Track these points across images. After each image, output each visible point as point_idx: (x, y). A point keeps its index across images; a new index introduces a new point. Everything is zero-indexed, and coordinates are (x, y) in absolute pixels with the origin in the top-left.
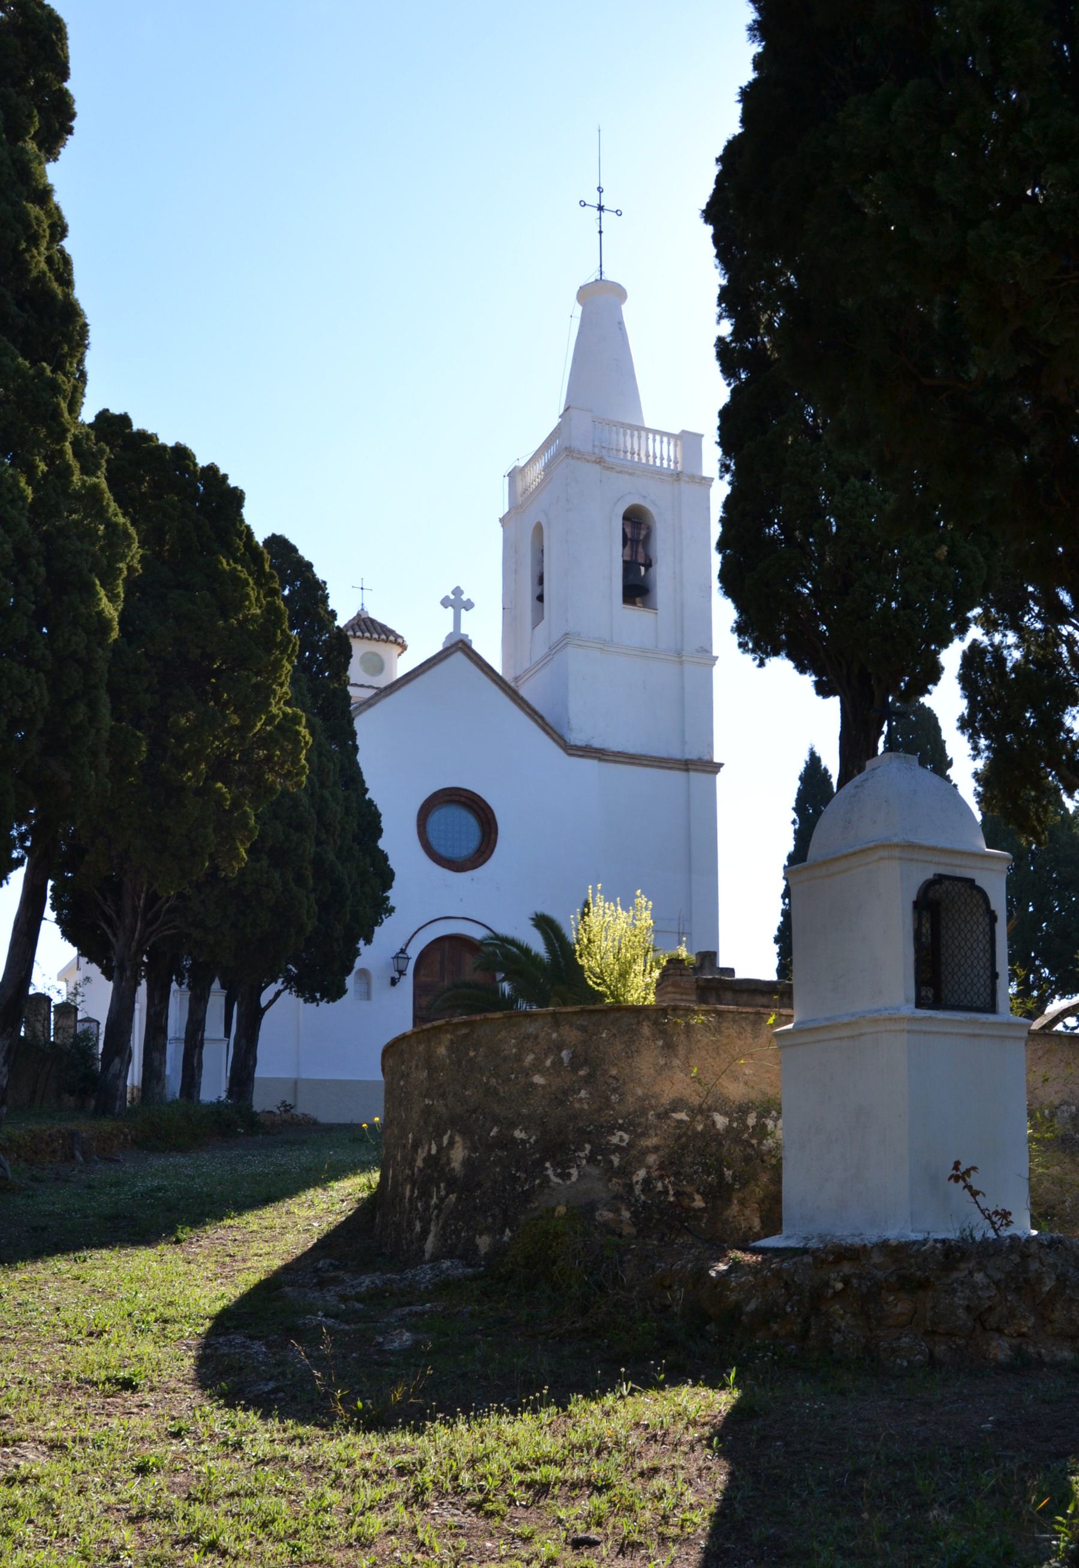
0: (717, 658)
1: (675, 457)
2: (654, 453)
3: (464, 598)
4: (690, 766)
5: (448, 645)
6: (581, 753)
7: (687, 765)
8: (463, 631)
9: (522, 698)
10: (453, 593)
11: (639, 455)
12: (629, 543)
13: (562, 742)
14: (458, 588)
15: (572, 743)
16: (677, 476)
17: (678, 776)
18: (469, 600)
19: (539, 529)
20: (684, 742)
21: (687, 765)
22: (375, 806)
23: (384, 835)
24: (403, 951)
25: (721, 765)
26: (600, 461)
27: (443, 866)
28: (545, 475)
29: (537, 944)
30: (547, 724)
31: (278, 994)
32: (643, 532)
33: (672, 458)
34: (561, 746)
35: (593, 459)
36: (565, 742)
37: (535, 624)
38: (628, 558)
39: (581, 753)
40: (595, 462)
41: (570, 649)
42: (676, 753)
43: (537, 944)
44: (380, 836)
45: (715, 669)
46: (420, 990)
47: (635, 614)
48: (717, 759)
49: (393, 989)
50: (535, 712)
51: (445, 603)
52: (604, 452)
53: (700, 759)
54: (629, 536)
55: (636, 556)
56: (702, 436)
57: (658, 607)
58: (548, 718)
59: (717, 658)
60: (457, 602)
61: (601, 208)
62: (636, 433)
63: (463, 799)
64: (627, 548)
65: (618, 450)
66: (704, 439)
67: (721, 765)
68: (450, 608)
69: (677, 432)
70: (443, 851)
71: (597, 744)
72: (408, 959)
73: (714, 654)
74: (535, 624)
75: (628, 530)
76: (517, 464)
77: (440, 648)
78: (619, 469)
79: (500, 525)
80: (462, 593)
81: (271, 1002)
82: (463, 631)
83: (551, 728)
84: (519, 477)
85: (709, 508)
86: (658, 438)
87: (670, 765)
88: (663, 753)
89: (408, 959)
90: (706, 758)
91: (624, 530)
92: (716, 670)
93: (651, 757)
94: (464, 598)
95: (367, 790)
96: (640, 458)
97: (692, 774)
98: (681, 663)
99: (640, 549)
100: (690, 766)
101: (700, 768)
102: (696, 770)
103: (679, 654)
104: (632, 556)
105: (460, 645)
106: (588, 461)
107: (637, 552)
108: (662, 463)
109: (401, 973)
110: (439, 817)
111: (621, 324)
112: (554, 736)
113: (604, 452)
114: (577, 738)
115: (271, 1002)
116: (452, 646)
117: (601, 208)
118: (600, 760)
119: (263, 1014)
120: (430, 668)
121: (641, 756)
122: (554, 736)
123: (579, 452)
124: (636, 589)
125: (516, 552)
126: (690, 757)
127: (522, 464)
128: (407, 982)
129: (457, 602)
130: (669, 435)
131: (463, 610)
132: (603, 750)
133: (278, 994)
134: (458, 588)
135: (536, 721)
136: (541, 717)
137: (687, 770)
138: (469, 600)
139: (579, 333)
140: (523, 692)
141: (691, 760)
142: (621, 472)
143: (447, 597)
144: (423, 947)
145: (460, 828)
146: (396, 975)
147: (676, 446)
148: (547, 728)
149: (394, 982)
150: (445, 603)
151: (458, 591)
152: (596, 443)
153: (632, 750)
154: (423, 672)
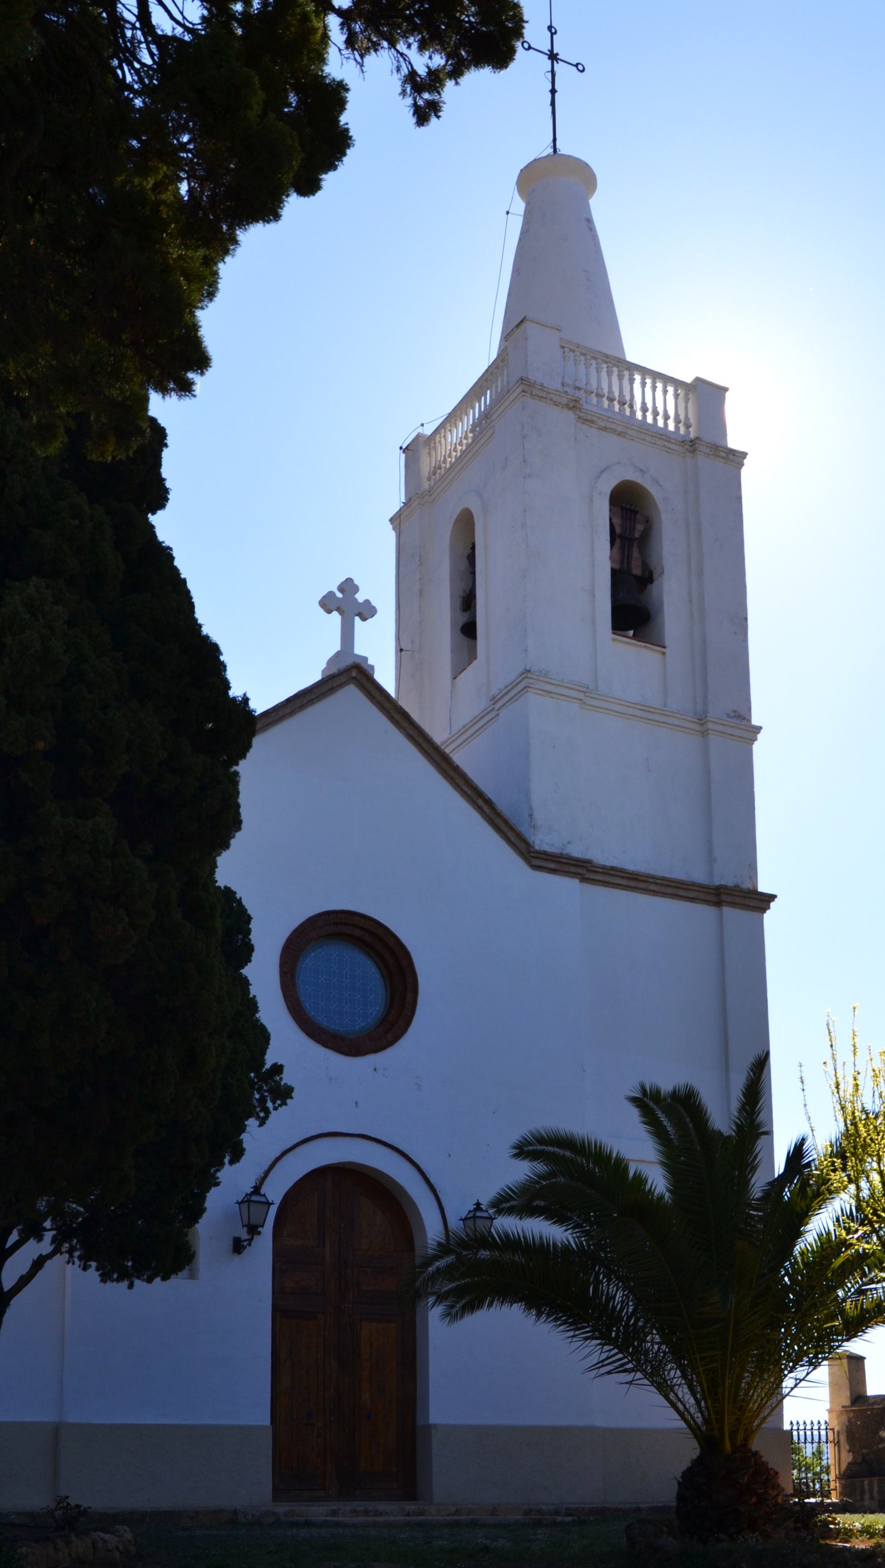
0: (759, 729)
1: (686, 417)
2: (644, 403)
3: (360, 597)
4: (724, 898)
5: (334, 670)
6: (553, 866)
7: (718, 895)
8: (359, 650)
9: (456, 769)
10: (341, 588)
11: (631, 406)
12: (618, 541)
13: (521, 845)
14: (349, 581)
15: (537, 848)
16: (692, 445)
17: (704, 913)
18: (367, 602)
19: (466, 523)
20: (711, 859)
21: (718, 895)
22: (239, 902)
23: (255, 956)
24: (257, 1190)
25: (773, 897)
26: (574, 406)
27: (326, 1045)
28: (474, 439)
29: (643, 1156)
30: (499, 815)
31: (38, 1264)
32: (640, 527)
33: (682, 417)
34: (520, 853)
35: (565, 401)
36: (527, 844)
37: (458, 670)
38: (617, 567)
39: (553, 866)
40: (567, 406)
41: (531, 697)
42: (698, 875)
43: (643, 1156)
44: (248, 960)
45: (757, 747)
46: (283, 1261)
47: (627, 653)
48: (763, 887)
49: (236, 1258)
50: (479, 794)
51: (328, 604)
52: (581, 395)
53: (737, 886)
54: (618, 530)
55: (629, 563)
56: (726, 390)
57: (667, 643)
58: (502, 804)
59: (759, 729)
60: (345, 603)
61: (553, 57)
62: (626, 373)
63: (358, 932)
64: (616, 549)
65: (600, 396)
66: (727, 394)
67: (773, 897)
68: (335, 614)
69: (689, 379)
70: (322, 1020)
71: (576, 851)
72: (269, 1204)
73: (755, 721)
74: (458, 670)
75: (617, 522)
76: (420, 430)
77: (317, 677)
78: (602, 424)
79: (390, 527)
80: (356, 589)
81: (24, 1281)
82: (359, 650)
83: (505, 821)
84: (424, 453)
85: (739, 498)
86: (659, 385)
87: (692, 894)
88: (678, 873)
89: (269, 1204)
90: (747, 885)
91: (610, 519)
92: (758, 748)
93: (663, 878)
94: (360, 597)
95: (216, 881)
96: (633, 412)
97: (727, 911)
98: (704, 733)
99: (635, 554)
100: (724, 898)
101: (737, 900)
102: (733, 904)
103: (702, 719)
104: (622, 562)
105: (354, 674)
106: (556, 404)
107: (629, 558)
108: (666, 424)
109: (253, 1230)
110: (318, 960)
111: (589, 221)
112: (510, 834)
113: (578, 394)
114: (543, 841)
115: (24, 1281)
116: (341, 673)
117: (553, 57)
118: (584, 880)
119: (7, 1304)
120: (303, 707)
121: (649, 876)
122: (510, 834)
123: (542, 387)
124: (633, 612)
125: (421, 563)
126: (723, 883)
127: (428, 431)
128: (263, 1246)
129: (345, 603)
130: (677, 383)
131: (357, 619)
132: (589, 862)
133: (38, 1264)
134: (349, 581)
135: (480, 809)
136: (489, 802)
137: (718, 904)
138: (367, 602)
139: (520, 240)
140: (458, 758)
141: (725, 887)
142: (605, 429)
143: (331, 594)
144: (290, 1184)
145: (354, 977)
146: (244, 1234)
147: (687, 400)
148: (498, 821)
149: (238, 1247)
150: (328, 604)
151: (348, 587)
152: (568, 380)
153: (630, 867)
154: (292, 714)
